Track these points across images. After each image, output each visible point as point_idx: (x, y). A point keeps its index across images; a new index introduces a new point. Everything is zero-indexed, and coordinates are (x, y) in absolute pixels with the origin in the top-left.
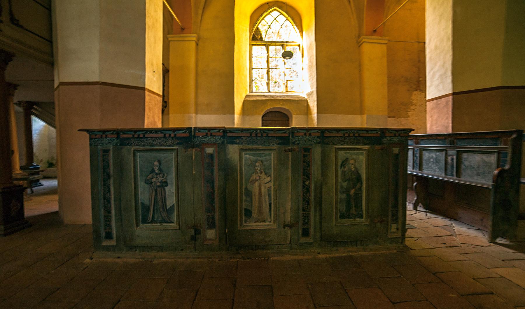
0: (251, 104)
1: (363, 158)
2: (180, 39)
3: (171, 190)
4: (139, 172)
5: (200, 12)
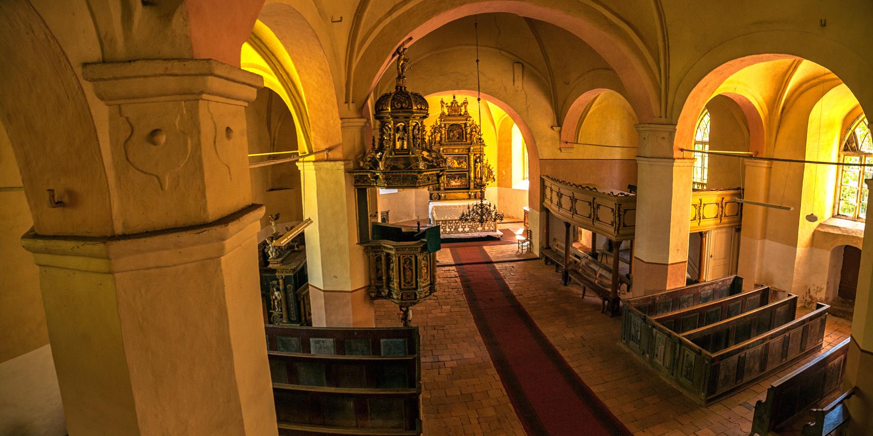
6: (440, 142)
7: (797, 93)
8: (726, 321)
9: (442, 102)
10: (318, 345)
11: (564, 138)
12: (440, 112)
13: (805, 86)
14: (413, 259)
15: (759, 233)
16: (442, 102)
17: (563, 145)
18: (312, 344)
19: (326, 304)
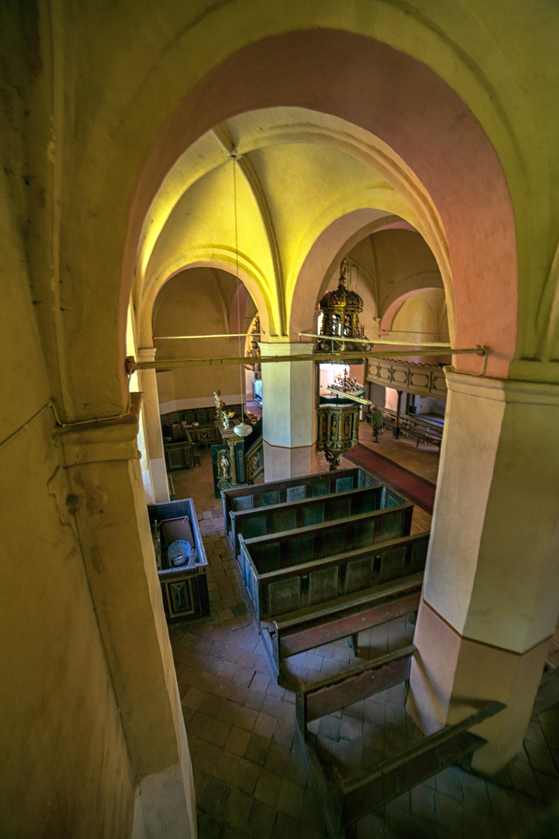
8: (180, 501)
10: (293, 494)
11: (382, 328)
14: (351, 417)
17: (382, 333)
18: (349, 478)
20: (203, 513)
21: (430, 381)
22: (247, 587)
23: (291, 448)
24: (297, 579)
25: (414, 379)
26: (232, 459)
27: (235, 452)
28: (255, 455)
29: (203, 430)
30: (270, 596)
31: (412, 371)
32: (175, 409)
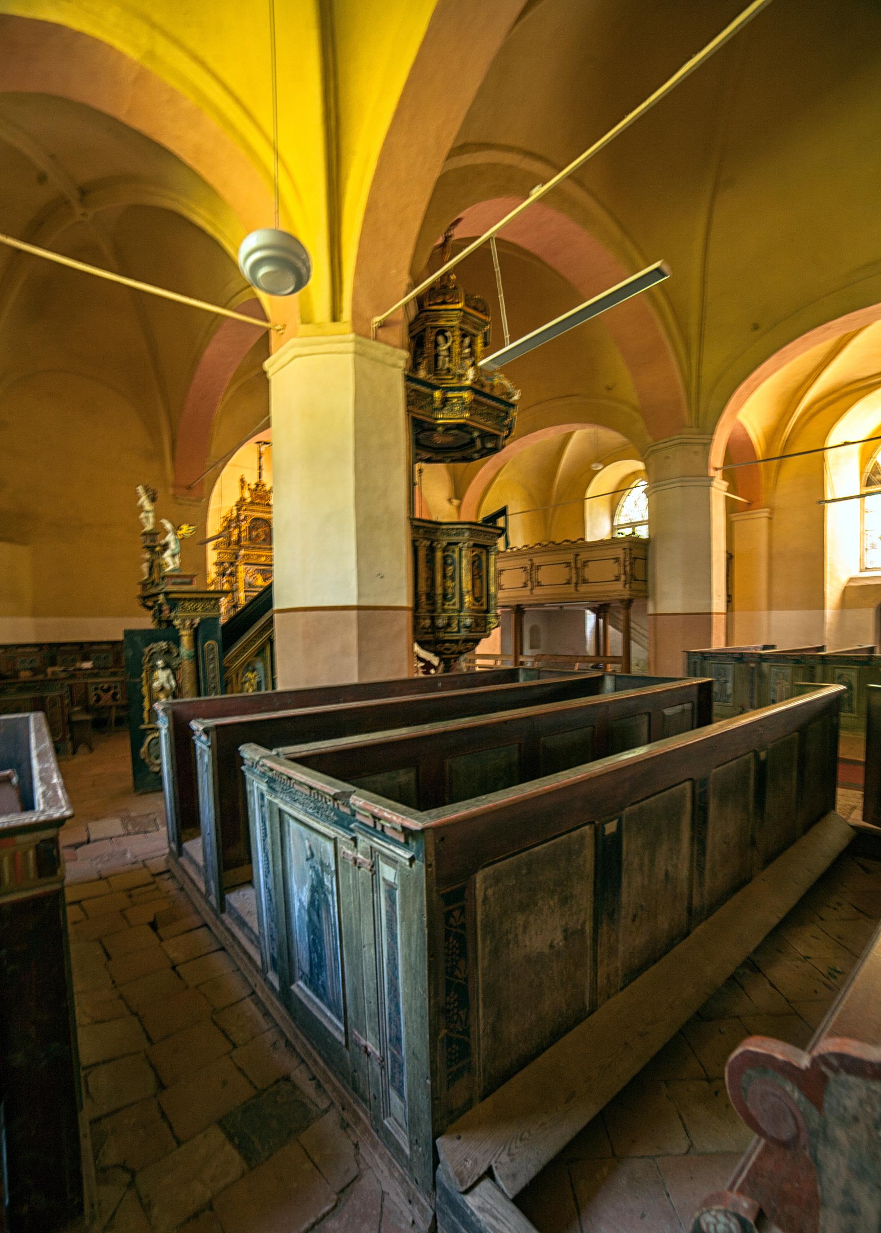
0: (852, 595)
1: (854, 674)
2: (747, 517)
3: (729, 685)
4: (257, 819)
5: (773, 474)
6: (238, 542)
7: (806, 417)
9: (242, 481)
12: (237, 498)
13: (817, 406)
15: (763, 601)
16: (242, 481)
19: (360, 637)
20: (90, 825)
21: (574, 571)
22: (300, 988)
23: (358, 608)
24: (582, 837)
25: (543, 576)
26: (187, 667)
27: (196, 647)
28: (249, 667)
29: (105, 681)
30: (483, 948)
31: (537, 561)
32: (30, 638)
